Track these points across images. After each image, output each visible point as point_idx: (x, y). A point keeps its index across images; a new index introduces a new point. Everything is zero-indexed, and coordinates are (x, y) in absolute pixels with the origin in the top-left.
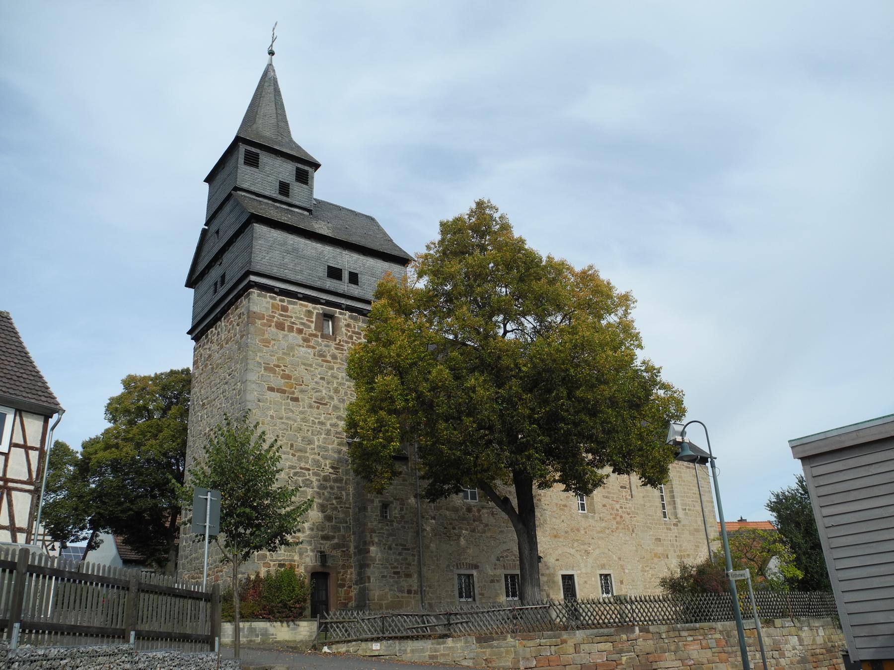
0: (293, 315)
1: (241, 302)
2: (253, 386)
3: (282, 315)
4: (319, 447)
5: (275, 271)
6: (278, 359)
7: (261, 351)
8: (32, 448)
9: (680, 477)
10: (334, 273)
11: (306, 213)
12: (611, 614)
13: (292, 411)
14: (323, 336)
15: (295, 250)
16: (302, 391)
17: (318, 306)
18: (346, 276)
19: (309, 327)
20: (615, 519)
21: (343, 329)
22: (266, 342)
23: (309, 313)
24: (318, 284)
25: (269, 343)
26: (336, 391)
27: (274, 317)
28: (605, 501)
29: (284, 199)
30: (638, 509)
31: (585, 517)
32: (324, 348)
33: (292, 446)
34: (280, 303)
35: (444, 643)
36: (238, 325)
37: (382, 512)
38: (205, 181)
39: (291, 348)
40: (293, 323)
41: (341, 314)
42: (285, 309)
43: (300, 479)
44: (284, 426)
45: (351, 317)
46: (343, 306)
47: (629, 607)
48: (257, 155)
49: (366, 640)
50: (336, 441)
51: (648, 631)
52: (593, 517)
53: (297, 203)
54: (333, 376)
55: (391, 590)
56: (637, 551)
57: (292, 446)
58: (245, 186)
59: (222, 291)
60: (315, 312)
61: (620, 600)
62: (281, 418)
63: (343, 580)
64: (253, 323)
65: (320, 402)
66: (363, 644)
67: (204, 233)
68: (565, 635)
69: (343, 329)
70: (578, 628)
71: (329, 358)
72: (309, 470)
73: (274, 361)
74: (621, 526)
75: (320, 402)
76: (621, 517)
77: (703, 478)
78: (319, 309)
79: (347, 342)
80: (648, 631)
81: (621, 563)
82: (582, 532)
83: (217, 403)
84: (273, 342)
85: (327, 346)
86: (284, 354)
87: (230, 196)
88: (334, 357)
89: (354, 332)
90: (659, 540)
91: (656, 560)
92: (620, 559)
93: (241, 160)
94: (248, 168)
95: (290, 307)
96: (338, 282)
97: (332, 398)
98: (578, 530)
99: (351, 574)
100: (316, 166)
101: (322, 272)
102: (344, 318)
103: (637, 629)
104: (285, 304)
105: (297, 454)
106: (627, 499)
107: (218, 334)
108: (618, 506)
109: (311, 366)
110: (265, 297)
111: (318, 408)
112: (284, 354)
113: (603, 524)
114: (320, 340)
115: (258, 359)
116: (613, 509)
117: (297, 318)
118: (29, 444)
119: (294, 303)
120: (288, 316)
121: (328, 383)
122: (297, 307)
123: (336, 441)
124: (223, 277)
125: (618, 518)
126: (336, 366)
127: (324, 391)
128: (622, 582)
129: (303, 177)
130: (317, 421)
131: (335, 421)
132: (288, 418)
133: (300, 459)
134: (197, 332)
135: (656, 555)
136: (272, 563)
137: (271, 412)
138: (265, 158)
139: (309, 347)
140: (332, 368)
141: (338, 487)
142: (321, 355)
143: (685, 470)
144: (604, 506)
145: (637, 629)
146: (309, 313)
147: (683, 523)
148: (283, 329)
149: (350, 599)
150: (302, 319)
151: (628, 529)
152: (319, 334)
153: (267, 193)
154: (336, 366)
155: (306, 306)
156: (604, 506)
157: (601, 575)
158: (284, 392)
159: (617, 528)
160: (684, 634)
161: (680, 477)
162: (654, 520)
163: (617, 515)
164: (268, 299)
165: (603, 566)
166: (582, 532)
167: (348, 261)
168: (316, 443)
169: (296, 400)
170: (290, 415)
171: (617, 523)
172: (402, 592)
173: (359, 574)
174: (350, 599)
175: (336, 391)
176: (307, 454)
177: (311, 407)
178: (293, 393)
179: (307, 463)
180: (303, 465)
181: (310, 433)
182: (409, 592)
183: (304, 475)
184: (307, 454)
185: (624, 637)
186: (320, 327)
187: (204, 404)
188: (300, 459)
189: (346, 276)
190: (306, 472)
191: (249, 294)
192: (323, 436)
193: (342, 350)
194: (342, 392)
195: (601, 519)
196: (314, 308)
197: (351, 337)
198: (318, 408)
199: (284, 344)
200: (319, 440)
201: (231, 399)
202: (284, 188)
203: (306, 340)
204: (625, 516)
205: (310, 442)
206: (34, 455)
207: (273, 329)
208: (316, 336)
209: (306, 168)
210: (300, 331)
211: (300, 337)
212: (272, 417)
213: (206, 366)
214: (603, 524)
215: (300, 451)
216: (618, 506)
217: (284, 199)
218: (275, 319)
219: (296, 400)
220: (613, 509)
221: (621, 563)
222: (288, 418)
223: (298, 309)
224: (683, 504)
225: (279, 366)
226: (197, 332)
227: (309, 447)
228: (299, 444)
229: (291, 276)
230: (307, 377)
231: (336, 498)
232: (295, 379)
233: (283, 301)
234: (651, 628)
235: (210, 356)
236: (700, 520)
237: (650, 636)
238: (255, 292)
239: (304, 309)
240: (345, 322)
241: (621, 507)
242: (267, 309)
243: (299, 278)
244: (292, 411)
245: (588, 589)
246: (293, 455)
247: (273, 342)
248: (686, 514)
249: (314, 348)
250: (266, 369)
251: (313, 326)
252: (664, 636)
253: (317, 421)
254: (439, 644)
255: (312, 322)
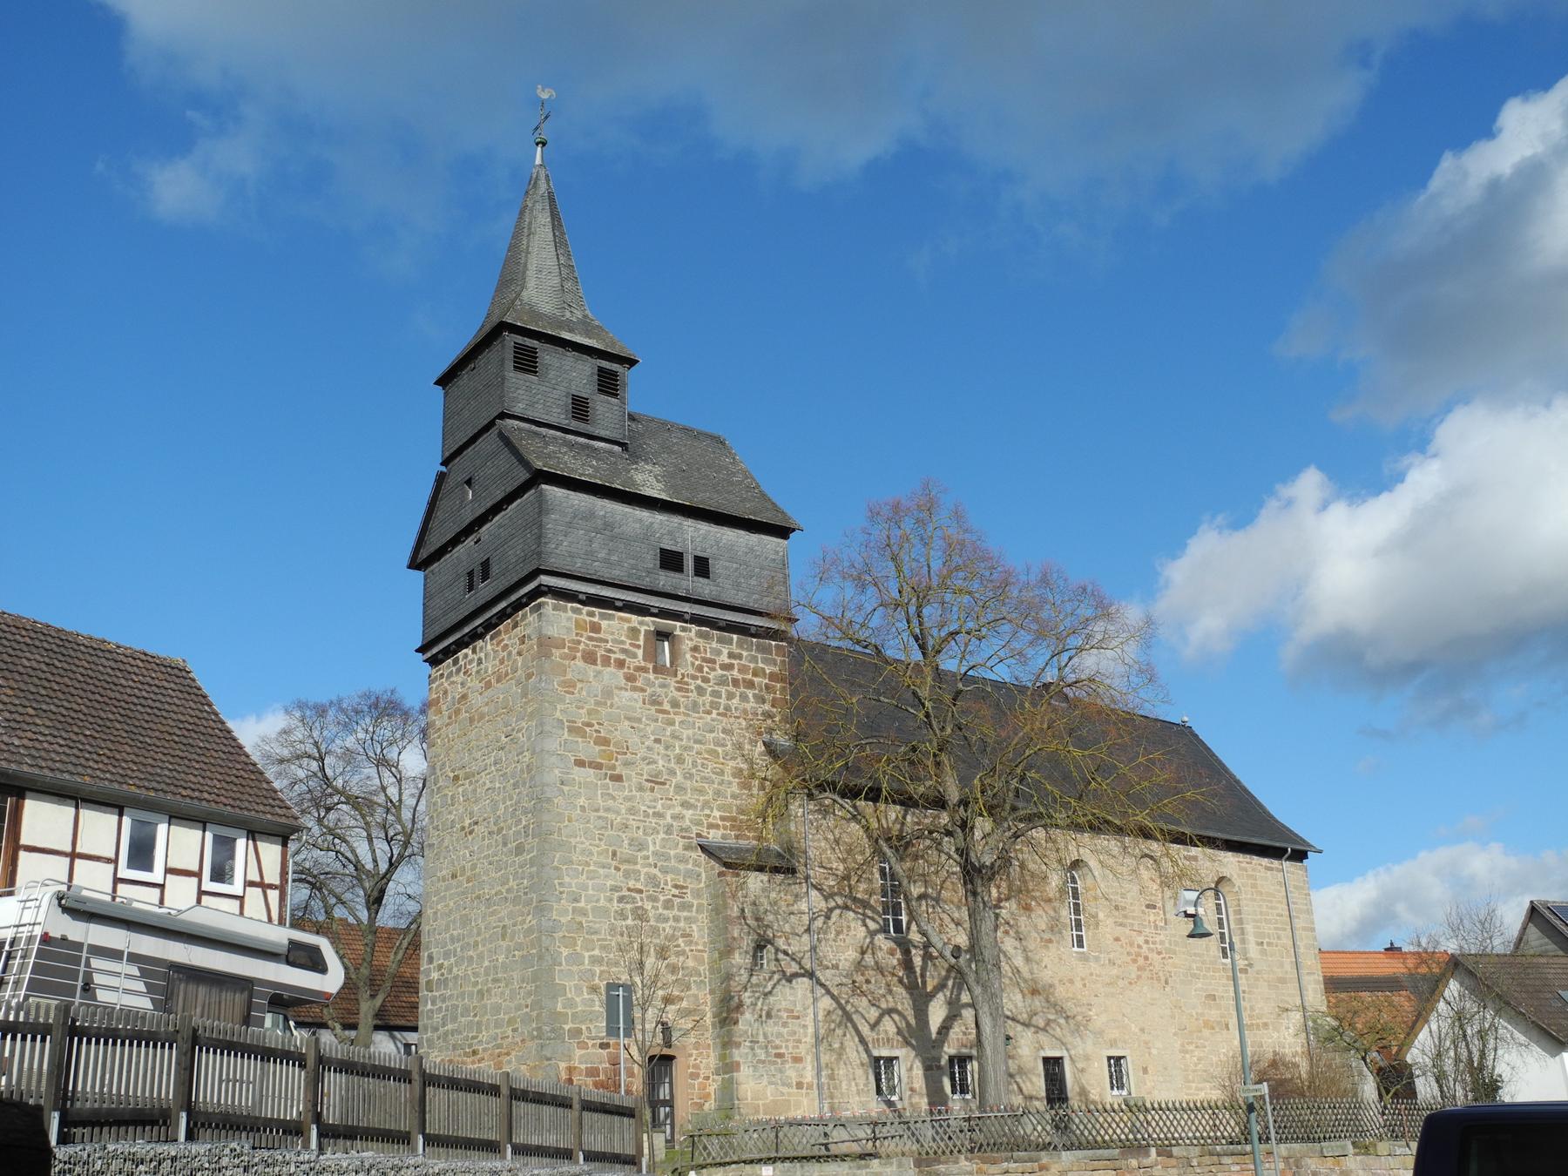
0: (610, 638)
1: (525, 616)
2: (554, 759)
3: (590, 639)
4: (655, 853)
5: (577, 567)
6: (589, 713)
7: (562, 700)
8: (271, 886)
9: (1254, 886)
10: (671, 560)
11: (617, 448)
12: (1119, 1129)
13: (614, 798)
14: (656, 670)
15: (608, 526)
16: (626, 764)
17: (648, 619)
18: (689, 564)
19: (635, 656)
20: (1135, 961)
21: (688, 656)
22: (570, 685)
23: (634, 632)
24: (645, 583)
25: (574, 686)
26: (680, 760)
27: (579, 642)
28: (1119, 931)
29: (581, 427)
30: (1176, 943)
31: (1084, 958)
32: (659, 690)
33: (614, 854)
34: (588, 619)
35: (867, 1167)
36: (519, 654)
37: (754, 956)
38: (437, 383)
39: (608, 693)
40: (610, 651)
41: (684, 629)
42: (596, 628)
43: (629, 906)
44: (601, 823)
45: (700, 635)
46: (687, 617)
47: (1141, 1117)
48: (534, 351)
49: (752, 1162)
50: (682, 842)
51: (1170, 1156)
52: (1097, 959)
53: (603, 433)
54: (674, 736)
55: (771, 1083)
56: (1173, 1017)
57: (614, 854)
58: (518, 409)
59: (486, 590)
60: (643, 629)
61: (1135, 1107)
62: (597, 810)
63: (696, 1067)
64: (548, 656)
65: (655, 781)
66: (748, 1167)
67: (441, 478)
68: (1045, 1157)
69: (688, 656)
70: (1067, 1148)
71: (667, 706)
72: (641, 891)
73: (582, 717)
74: (1146, 974)
75: (655, 781)
76: (1146, 958)
77: (1296, 887)
78: (650, 623)
79: (694, 678)
80: (1170, 1156)
81: (1145, 1037)
82: (1079, 984)
83: (484, 778)
84: (579, 685)
85: (663, 686)
86: (598, 703)
87: (491, 424)
88: (675, 704)
89: (705, 660)
90: (1213, 998)
91: (1206, 1032)
92: (1142, 1030)
93: (510, 364)
94: (521, 375)
95: (604, 624)
96: (677, 575)
97: (672, 773)
98: (1071, 981)
99: (710, 1060)
100: (632, 362)
101: (651, 560)
102: (689, 635)
103: (1153, 1151)
104: (596, 619)
105: (623, 867)
106: (1156, 927)
107: (480, 662)
108: (1140, 940)
109: (639, 720)
110: (565, 610)
111: (652, 790)
112: (598, 703)
113: (1115, 971)
114: (652, 676)
115: (558, 714)
116: (1132, 945)
117: (615, 641)
118: (267, 881)
119: (610, 618)
120: (602, 640)
121: (667, 748)
122: (615, 623)
123: (682, 842)
124: (486, 566)
125: (1141, 961)
126: (678, 719)
127: (661, 762)
128: (1145, 1071)
129: (608, 384)
130: (651, 811)
131: (678, 809)
132: (608, 810)
133: (627, 875)
134: (435, 650)
135: (1207, 1024)
136: (590, 1043)
137: (582, 801)
138: (548, 357)
139: (635, 689)
140: (672, 723)
141: (686, 919)
142: (655, 702)
143: (1262, 873)
144: (1117, 939)
145: (1153, 1151)
146: (634, 632)
147: (1256, 968)
148: (594, 662)
149: (706, 1097)
150: (623, 642)
151: (1159, 980)
152: (651, 666)
153: (553, 420)
154: (678, 719)
155: (629, 621)
156: (1117, 939)
157: (1109, 1058)
158: (599, 766)
159: (1139, 977)
160: (1226, 1160)
161: (1254, 886)
162: (1203, 962)
163: (1139, 955)
164: (570, 613)
165: (1113, 1043)
166: (1079, 984)
167: (693, 536)
168: (651, 848)
169: (618, 778)
170: (610, 802)
171: (1139, 969)
172: (789, 1085)
173: (722, 1057)
174: (706, 1097)
175: (680, 760)
176: (638, 867)
177: (641, 789)
178: (613, 768)
179: (637, 880)
180: (631, 884)
181: (641, 832)
182: (799, 1085)
183: (634, 900)
184: (638, 867)
185: (1134, 1163)
186: (652, 655)
187: (456, 778)
188: (627, 875)
189: (689, 564)
190: (638, 896)
191: (539, 606)
192: (662, 835)
193: (687, 691)
194: (689, 760)
195: (1112, 963)
196: (641, 623)
197: (700, 669)
198: (652, 790)
199: (597, 687)
200: (654, 843)
201: (513, 776)
202: (580, 407)
203: (630, 678)
204: (1154, 956)
205: (642, 846)
206: (274, 895)
207: (579, 663)
208: (645, 670)
209: (615, 367)
210: (621, 664)
211: (621, 673)
212: (583, 808)
213: (457, 712)
214: (1115, 971)
215: (628, 861)
216: (1140, 940)
217: (581, 427)
218: (582, 647)
219: (618, 778)
220: (1132, 945)
221: (1145, 1037)
222: (608, 810)
223: (617, 626)
224: (1257, 935)
225: (589, 725)
226: (435, 650)
227: (639, 854)
228: (625, 850)
229: (606, 574)
230: (634, 739)
231: (683, 936)
232: (615, 745)
233: (591, 614)
234: (1175, 1150)
235: (464, 697)
236: (1288, 962)
237: (1173, 1161)
238: (548, 601)
239: (626, 625)
240: (690, 644)
241: (1147, 942)
242: (569, 629)
243: (616, 574)
244: (614, 798)
245: (1088, 1078)
246: (617, 869)
247: (579, 685)
248: (1264, 952)
249: (643, 690)
250: (571, 730)
251: (640, 653)
252: (1195, 1163)
253: (651, 811)
254: (859, 1168)
255: (638, 647)
